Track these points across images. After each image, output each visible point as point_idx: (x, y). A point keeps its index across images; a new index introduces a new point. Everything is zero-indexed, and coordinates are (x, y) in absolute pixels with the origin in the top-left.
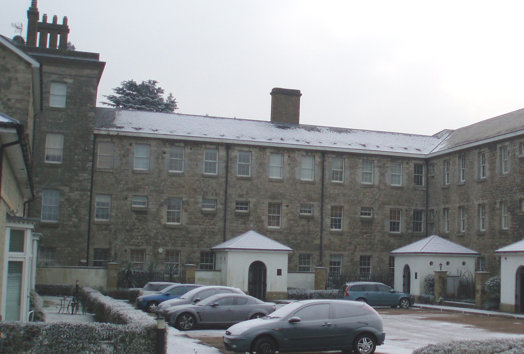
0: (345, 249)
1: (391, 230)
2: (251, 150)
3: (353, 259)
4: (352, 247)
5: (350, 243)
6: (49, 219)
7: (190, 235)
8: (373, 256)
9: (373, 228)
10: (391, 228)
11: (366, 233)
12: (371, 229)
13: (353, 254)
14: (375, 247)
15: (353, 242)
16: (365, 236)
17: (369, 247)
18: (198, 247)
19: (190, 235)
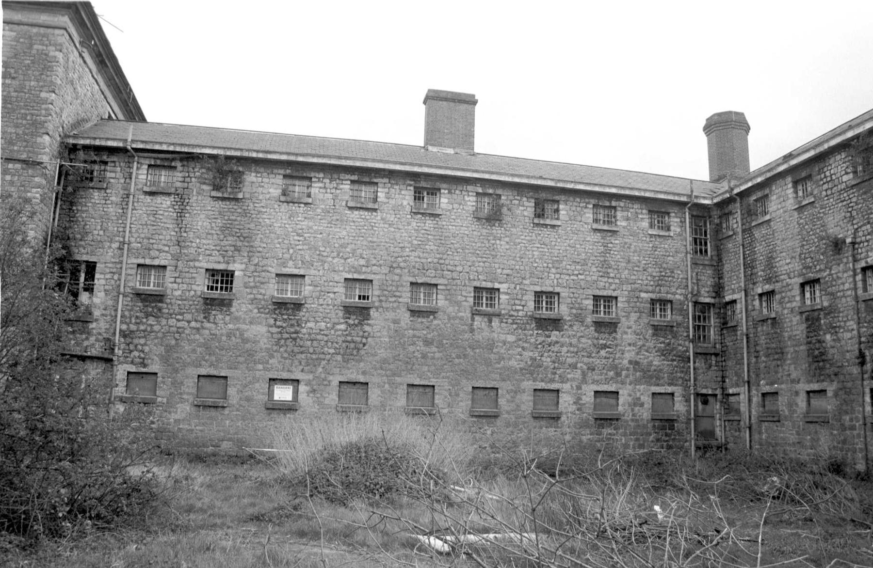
0: (563, 380)
1: (346, 298)
2: (499, 192)
3: (579, 399)
4: (578, 374)
5: (574, 366)
6: (690, 401)
7: (248, 346)
8: (621, 392)
9: (619, 336)
10: (232, 276)
11: (605, 347)
12: (615, 338)
13: (579, 388)
14: (624, 373)
15: (579, 365)
16: (603, 353)
17: (612, 373)
18: (265, 369)
19: (248, 346)
